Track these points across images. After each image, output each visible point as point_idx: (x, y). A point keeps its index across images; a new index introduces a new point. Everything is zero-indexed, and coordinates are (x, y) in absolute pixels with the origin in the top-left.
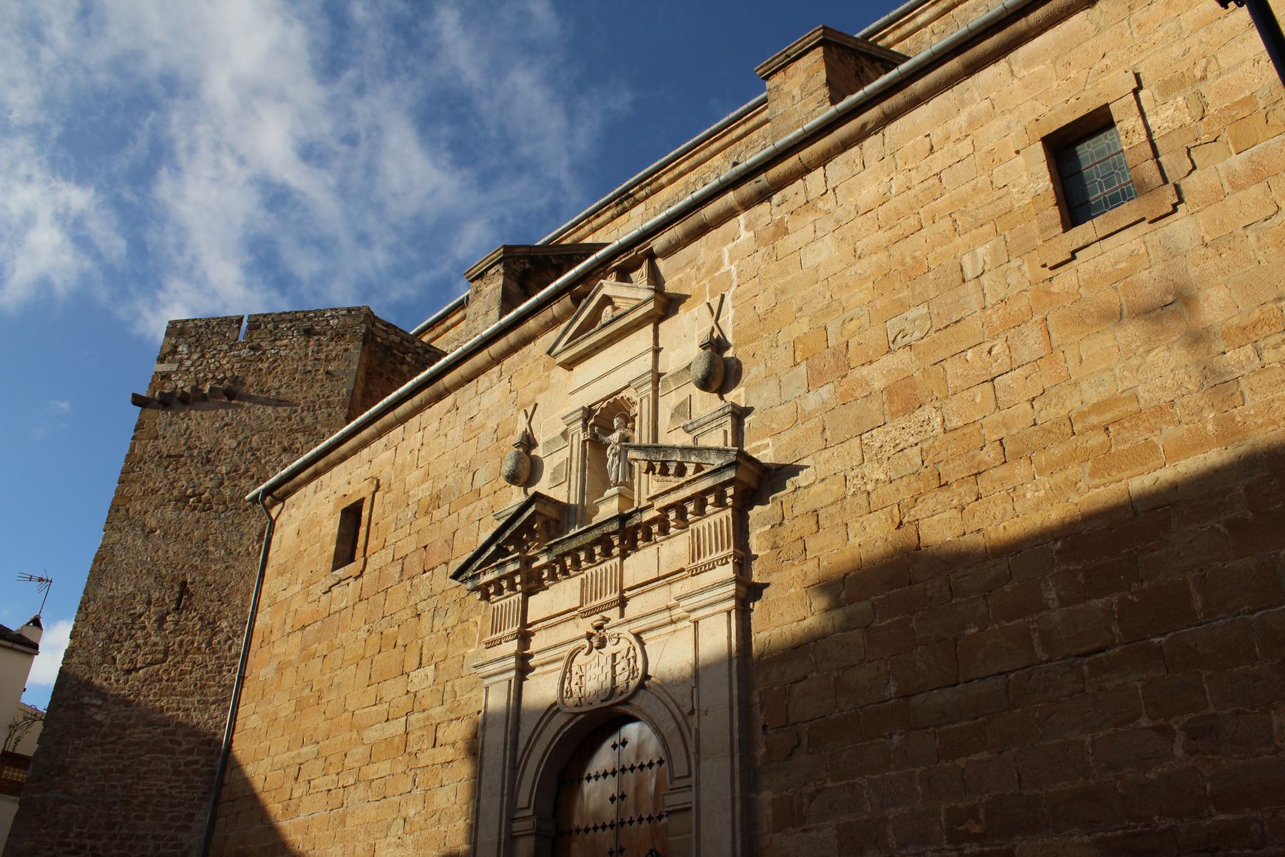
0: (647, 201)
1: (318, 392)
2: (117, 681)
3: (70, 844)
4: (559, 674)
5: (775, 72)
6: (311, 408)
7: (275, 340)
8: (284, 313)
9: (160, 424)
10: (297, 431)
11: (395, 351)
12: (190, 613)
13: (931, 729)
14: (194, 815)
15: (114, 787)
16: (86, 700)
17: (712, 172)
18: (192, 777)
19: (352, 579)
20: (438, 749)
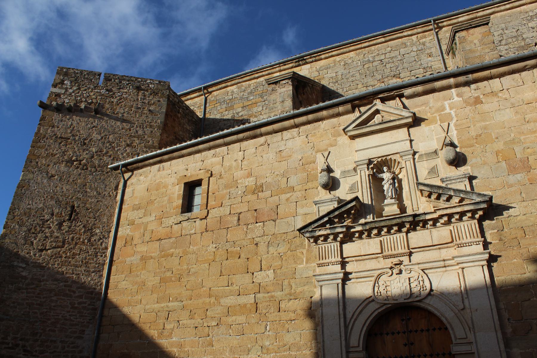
0: (312, 64)
1: (145, 119)
2: (35, 255)
3: (9, 343)
4: (372, 283)
5: (462, 30)
7: (120, 88)
8: (124, 76)
9: (55, 120)
10: (134, 137)
11: (176, 106)
12: (78, 223)
14: (84, 331)
15: (36, 313)
16: (15, 263)
17: (350, 59)
18: (82, 310)
19: (198, 219)
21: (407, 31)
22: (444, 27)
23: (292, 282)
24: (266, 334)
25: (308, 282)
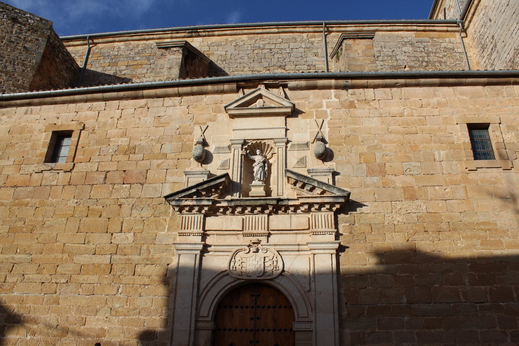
0: (204, 38)
4: (229, 258)
5: (350, 39)
6: (12, 62)
11: (56, 50)
13: (421, 317)
19: (62, 171)
20: (136, 277)
21: (299, 27)
22: (333, 31)
23: (151, 248)
24: (117, 296)
25: (167, 249)
